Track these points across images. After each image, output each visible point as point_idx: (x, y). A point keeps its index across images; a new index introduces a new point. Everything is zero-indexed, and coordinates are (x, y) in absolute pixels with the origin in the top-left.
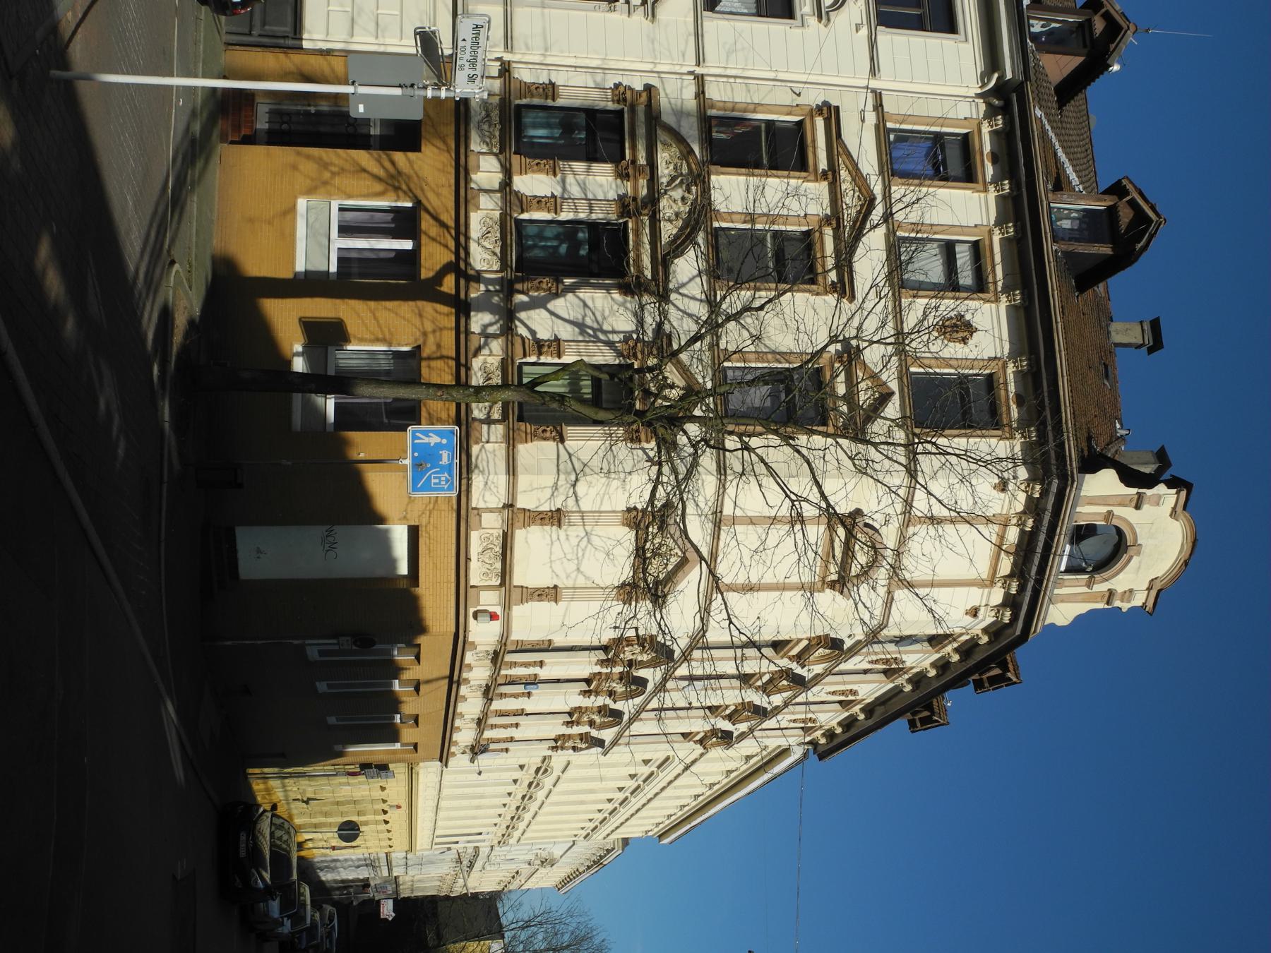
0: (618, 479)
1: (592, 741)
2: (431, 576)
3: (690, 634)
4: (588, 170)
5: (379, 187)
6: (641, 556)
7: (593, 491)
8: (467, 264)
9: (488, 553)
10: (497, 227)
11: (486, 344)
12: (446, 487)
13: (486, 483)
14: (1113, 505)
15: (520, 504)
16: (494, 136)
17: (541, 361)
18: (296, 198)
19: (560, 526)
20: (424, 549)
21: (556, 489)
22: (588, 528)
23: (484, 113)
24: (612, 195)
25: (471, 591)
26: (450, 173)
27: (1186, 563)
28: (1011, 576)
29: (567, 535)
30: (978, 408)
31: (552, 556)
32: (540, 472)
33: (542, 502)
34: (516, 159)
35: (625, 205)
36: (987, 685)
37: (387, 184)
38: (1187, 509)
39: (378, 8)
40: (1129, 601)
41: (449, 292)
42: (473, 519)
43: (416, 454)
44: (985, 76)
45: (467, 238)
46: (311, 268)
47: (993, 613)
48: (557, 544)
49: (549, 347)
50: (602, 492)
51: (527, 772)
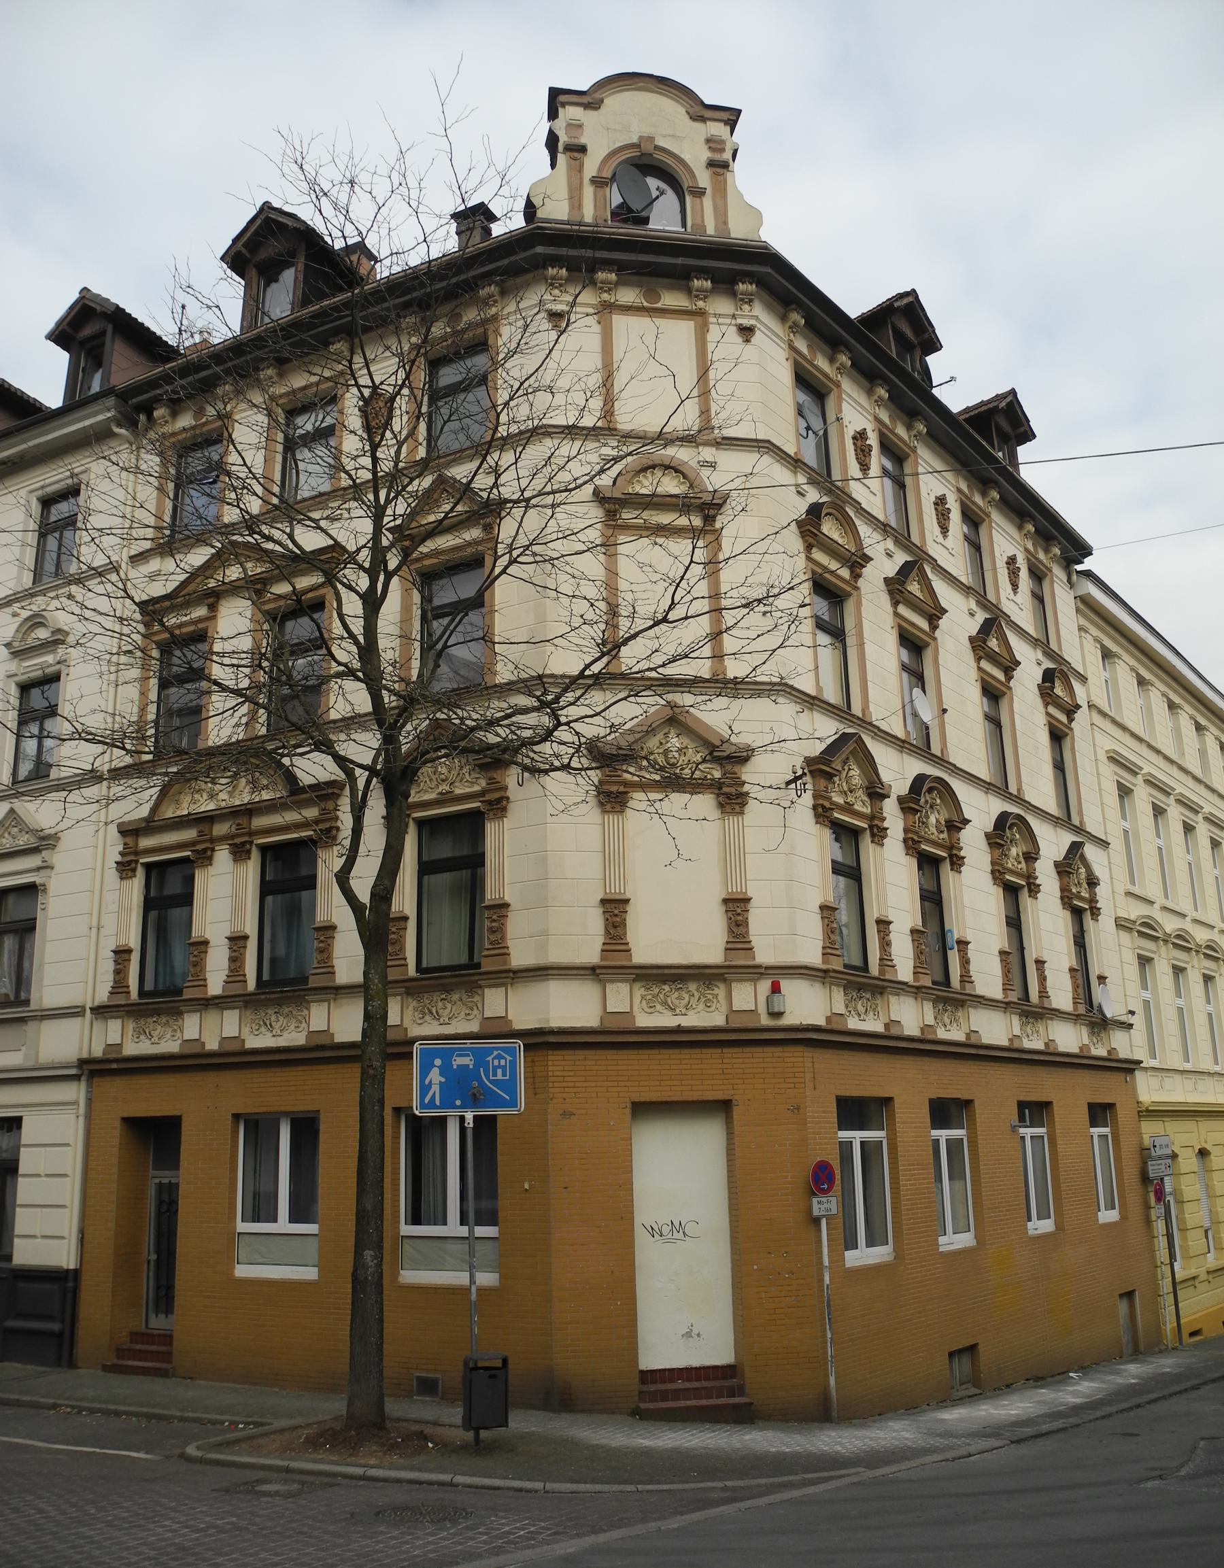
1: (1070, 859)
2: (713, 1082)
3: (798, 707)
6: (673, 782)
12: (509, 1058)
14: (581, 179)
25: (735, 1024)
28: (689, 291)
34: (188, 994)
51: (1187, 963)
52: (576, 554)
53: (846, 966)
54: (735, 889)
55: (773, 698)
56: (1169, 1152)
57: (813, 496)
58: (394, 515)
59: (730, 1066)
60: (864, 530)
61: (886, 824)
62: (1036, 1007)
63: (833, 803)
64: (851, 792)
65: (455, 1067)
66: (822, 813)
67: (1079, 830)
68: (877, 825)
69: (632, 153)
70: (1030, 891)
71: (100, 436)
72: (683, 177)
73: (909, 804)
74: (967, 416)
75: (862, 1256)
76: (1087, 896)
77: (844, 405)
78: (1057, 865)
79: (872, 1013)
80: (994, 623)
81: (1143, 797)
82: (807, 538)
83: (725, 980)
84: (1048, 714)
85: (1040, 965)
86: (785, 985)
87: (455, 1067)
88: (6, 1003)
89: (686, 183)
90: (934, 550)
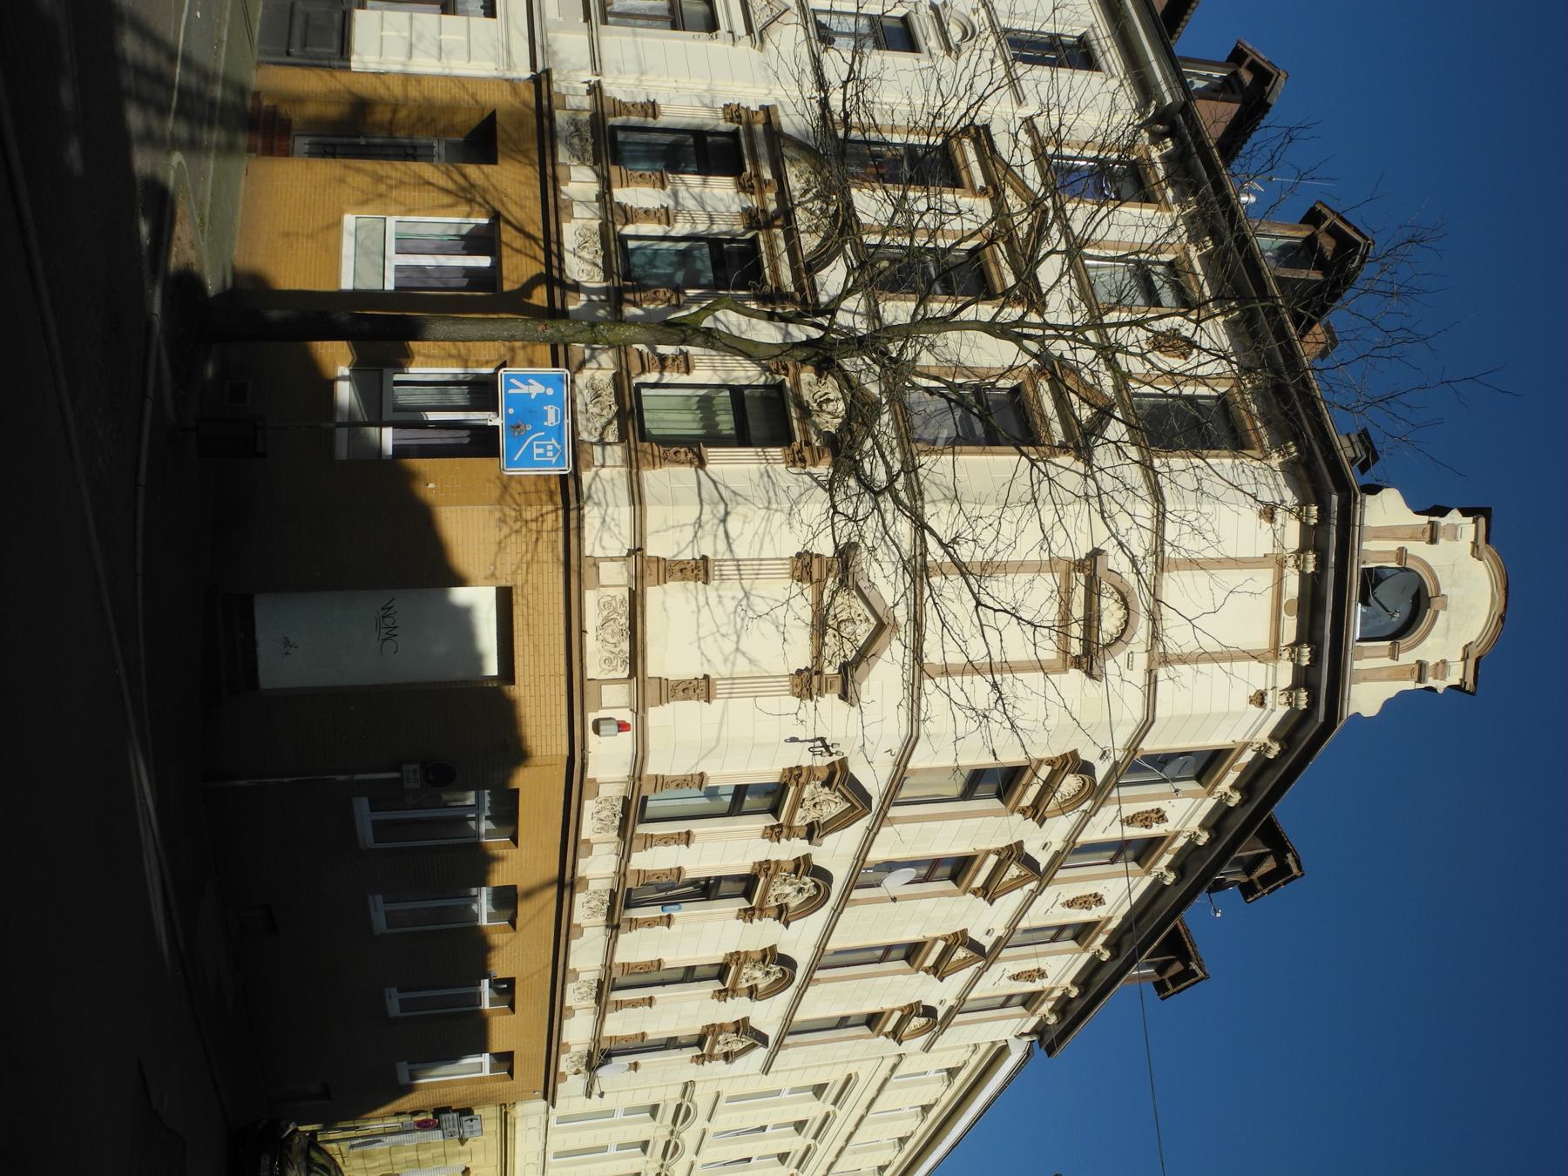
0: (781, 511)
4: (705, 183)
5: (447, 200)
6: (820, 626)
7: (749, 530)
8: (561, 270)
9: (612, 626)
10: (597, 238)
11: (592, 357)
12: (554, 460)
13: (604, 521)
14: (1403, 539)
15: (651, 551)
16: (587, 151)
17: (664, 381)
18: (342, 213)
19: (706, 583)
20: (520, 624)
21: (700, 526)
22: (746, 584)
23: (572, 128)
24: (736, 208)
25: (589, 686)
26: (534, 186)
27: (1502, 618)
29: (720, 597)
30: (1213, 427)
31: (700, 631)
32: (675, 502)
33: (683, 546)
34: (615, 171)
35: (754, 219)
36: (1259, 887)
37: (457, 196)
38: (1491, 540)
39: (440, 34)
40: (1444, 678)
41: (540, 304)
42: (588, 572)
43: (511, 411)
44: (1142, 106)
45: (560, 244)
46: (361, 286)
47: (1284, 699)
48: (705, 611)
49: (674, 361)
50: (761, 531)
51: (661, 1122)
52: (1041, 524)
53: (614, 979)
54: (720, 688)
55: (904, 703)
56: (467, 1135)
57: (1101, 770)
58: (1075, 348)
59: (547, 683)
60: (1074, 817)
61: (783, 840)
62: (607, 997)
63: (803, 786)
64: (815, 805)
65: (545, 408)
66: (795, 774)
67: (779, 1043)
68: (781, 832)
69: (1431, 592)
70: (720, 991)
71: (1144, 87)
72: (1408, 639)
73: (803, 866)
74: (1182, 931)
75: (364, 815)
76: (716, 1051)
77: (1191, 800)
78: (745, 1020)
79: (599, 826)
80: (983, 955)
81: (813, 1110)
82: (1060, 761)
83: (630, 677)
84: (892, 1011)
85: (647, 1001)
86: (627, 738)
87: (545, 408)
88: (604, 5)
89: (1403, 643)
90: (1050, 893)
